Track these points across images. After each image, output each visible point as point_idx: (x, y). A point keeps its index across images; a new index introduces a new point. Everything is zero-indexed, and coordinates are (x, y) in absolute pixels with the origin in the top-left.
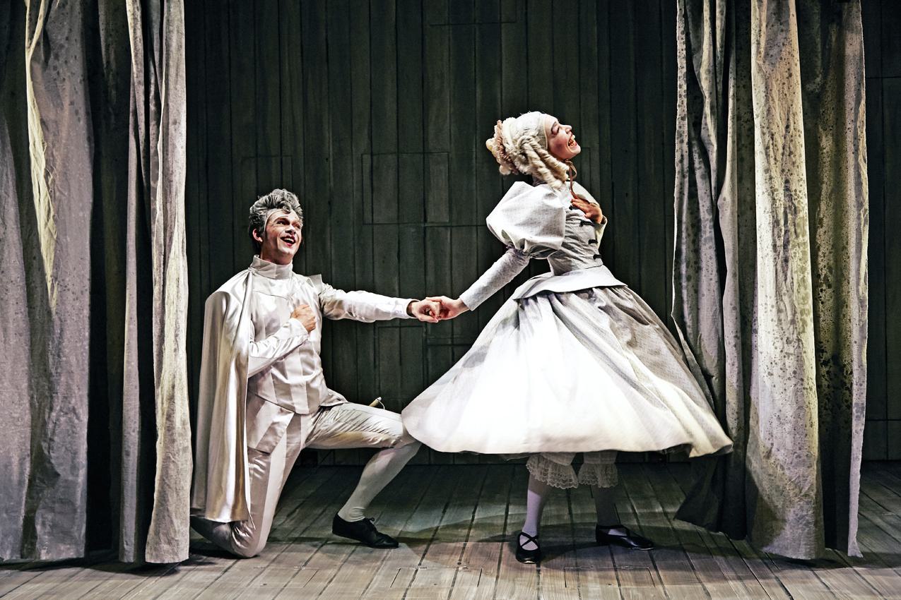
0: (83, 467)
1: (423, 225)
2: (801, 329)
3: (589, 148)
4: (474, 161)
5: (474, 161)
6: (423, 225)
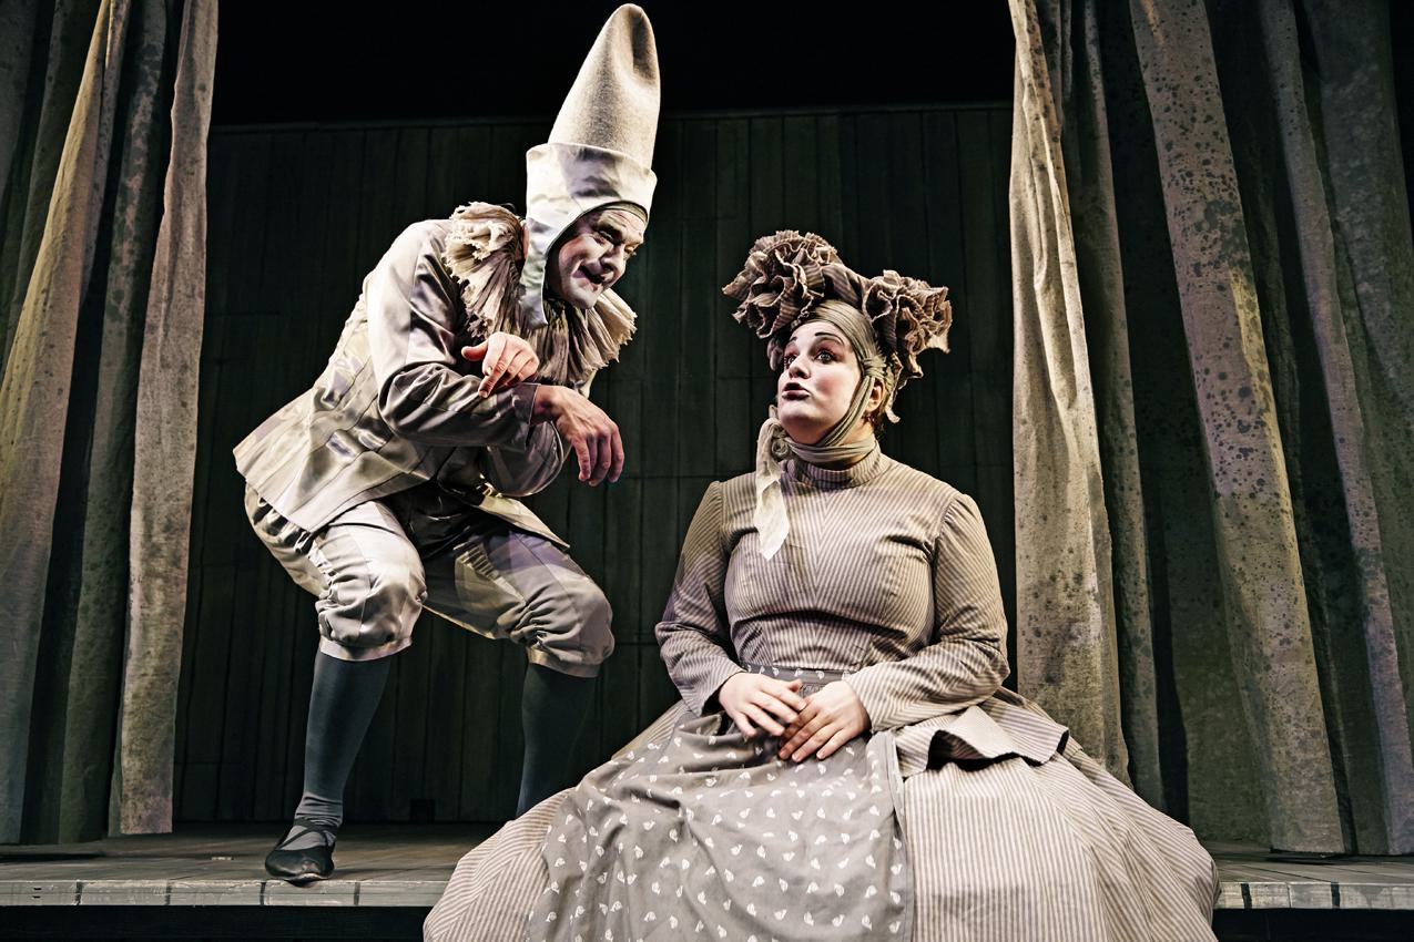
0: (1369, 901)
2: (1264, 406)
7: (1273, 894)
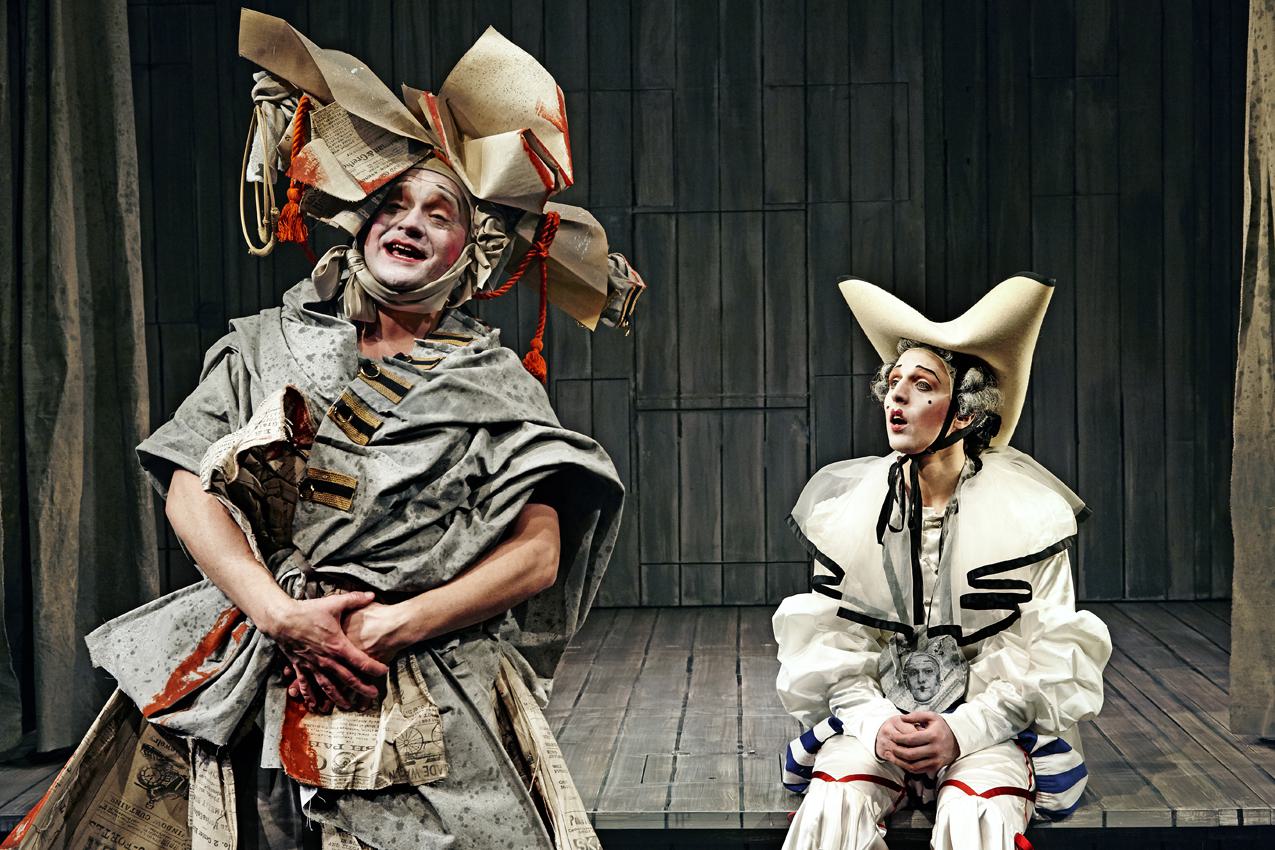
1: (630, 211)
3: (907, 83)
4: (716, 104)
5: (716, 104)
6: (630, 211)
7: (1259, 816)
